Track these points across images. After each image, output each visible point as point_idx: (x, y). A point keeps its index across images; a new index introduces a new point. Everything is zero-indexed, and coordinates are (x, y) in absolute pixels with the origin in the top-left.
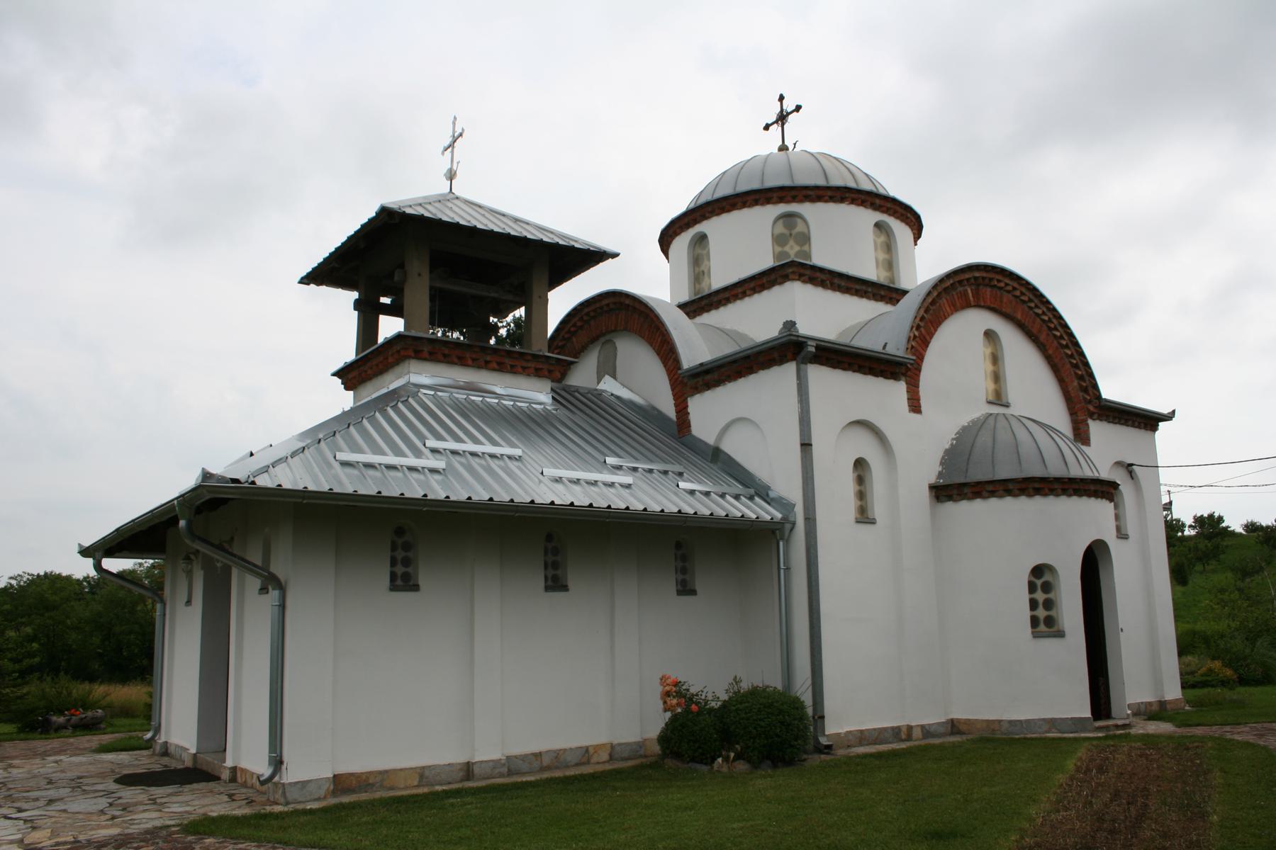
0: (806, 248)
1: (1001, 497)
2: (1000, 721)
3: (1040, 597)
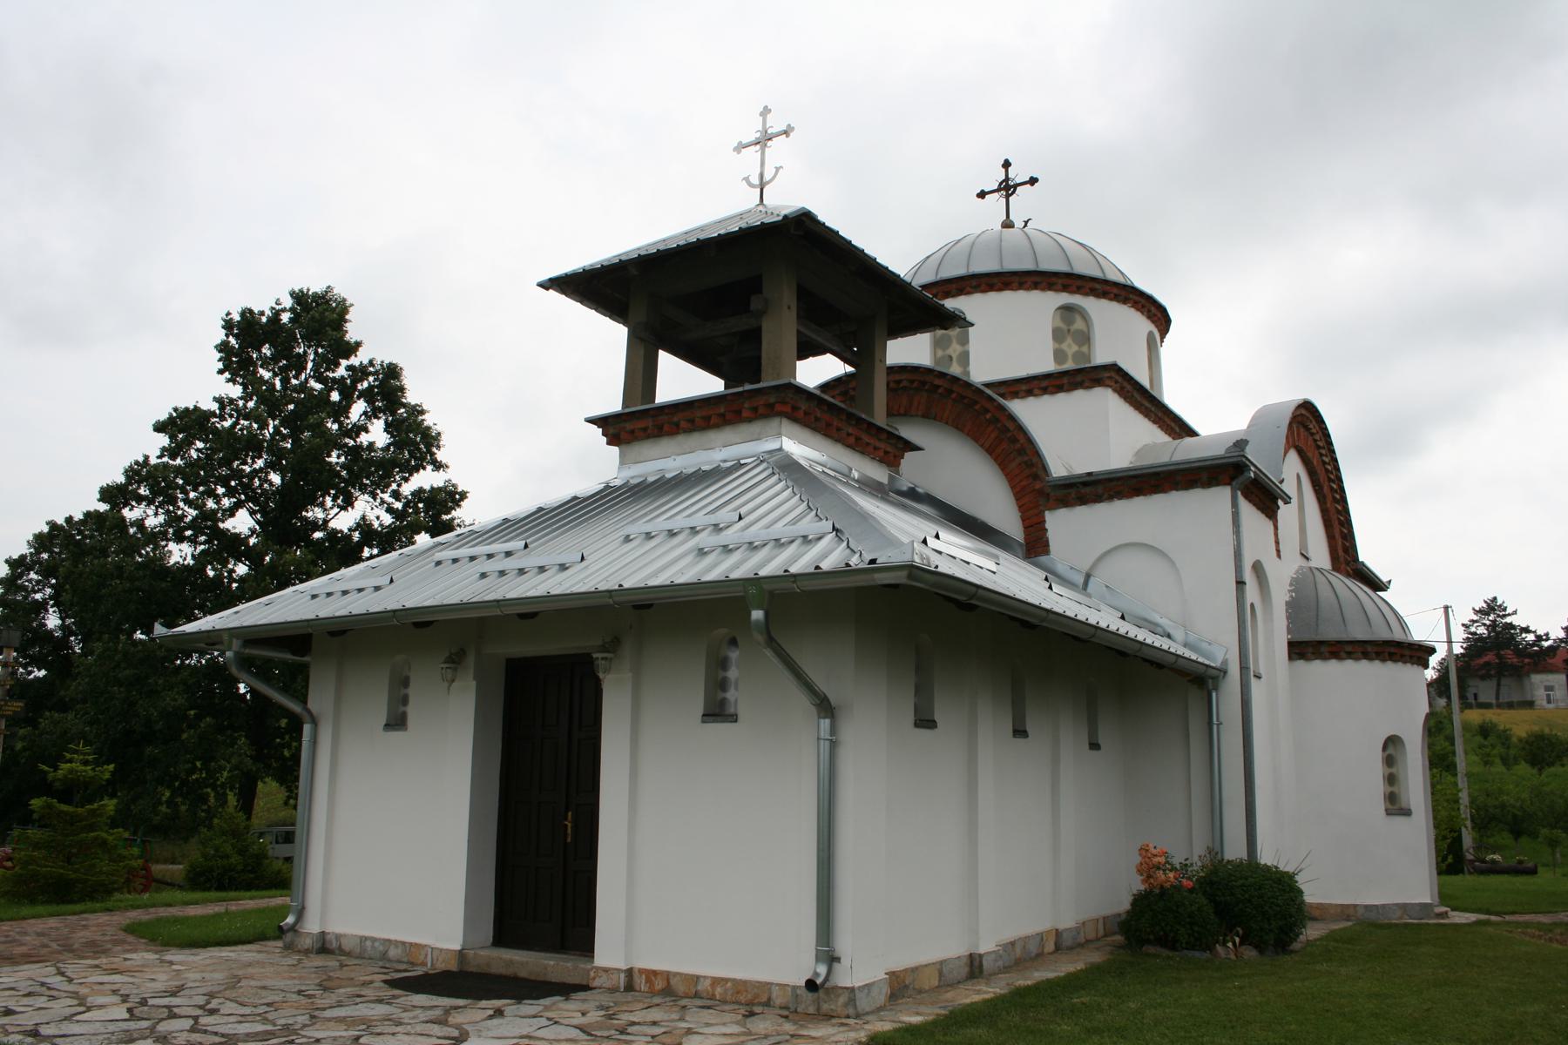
0: (1085, 349)
1: (1357, 659)
2: (1355, 906)
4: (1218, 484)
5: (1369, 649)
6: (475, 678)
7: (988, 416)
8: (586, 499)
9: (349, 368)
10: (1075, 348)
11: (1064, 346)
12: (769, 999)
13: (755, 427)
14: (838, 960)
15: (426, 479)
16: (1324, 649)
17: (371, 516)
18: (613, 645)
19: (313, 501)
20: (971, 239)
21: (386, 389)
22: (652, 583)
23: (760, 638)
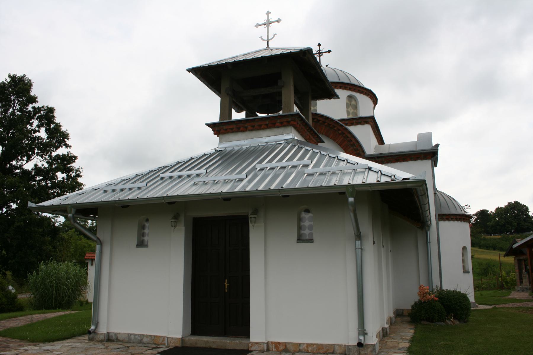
1: (454, 221)
4: (426, 159)
5: (458, 217)
6: (184, 226)
7: (340, 132)
8: (211, 155)
9: (34, 107)
10: (352, 111)
11: (349, 110)
12: (334, 351)
13: (281, 130)
14: (366, 334)
15: (62, 151)
16: (444, 217)
17: (40, 165)
18: (256, 212)
19: (15, 158)
21: (47, 116)
22: (207, 192)
23: (351, 208)
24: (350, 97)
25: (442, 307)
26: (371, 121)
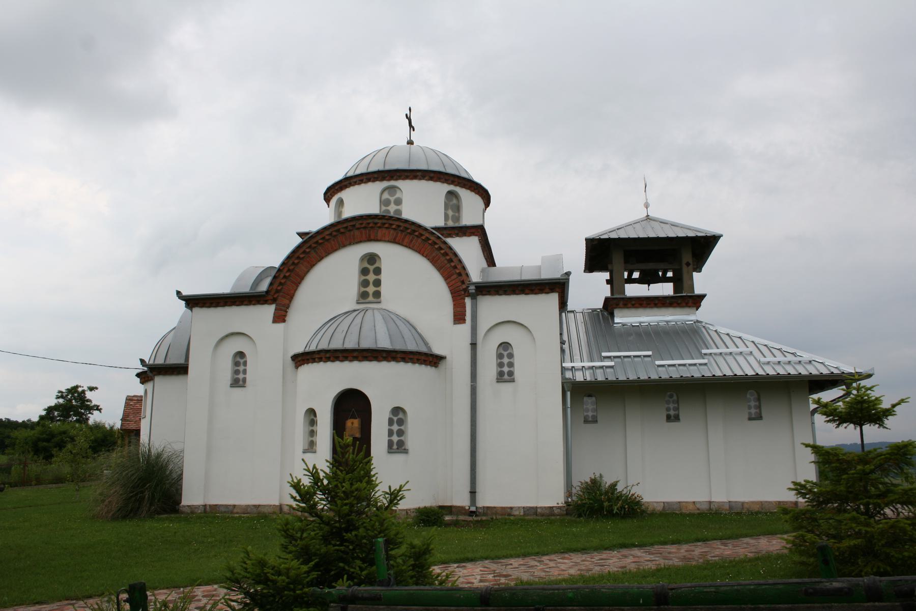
3: (395, 428)
20: (382, 154)
24: (450, 193)
25: (785, 536)
26: (479, 231)
